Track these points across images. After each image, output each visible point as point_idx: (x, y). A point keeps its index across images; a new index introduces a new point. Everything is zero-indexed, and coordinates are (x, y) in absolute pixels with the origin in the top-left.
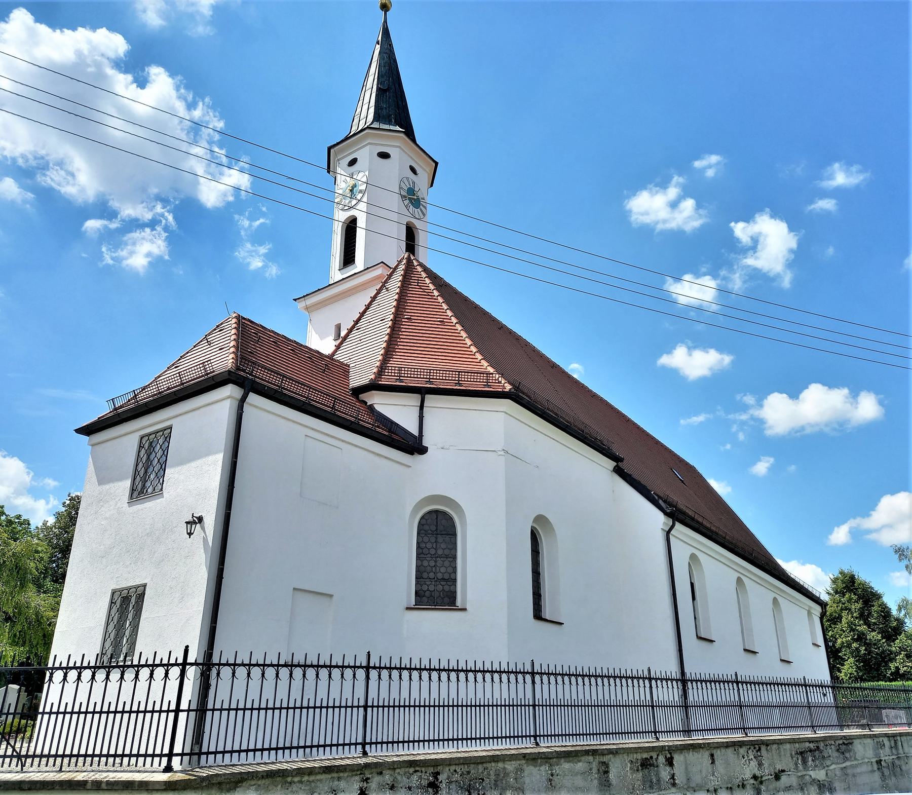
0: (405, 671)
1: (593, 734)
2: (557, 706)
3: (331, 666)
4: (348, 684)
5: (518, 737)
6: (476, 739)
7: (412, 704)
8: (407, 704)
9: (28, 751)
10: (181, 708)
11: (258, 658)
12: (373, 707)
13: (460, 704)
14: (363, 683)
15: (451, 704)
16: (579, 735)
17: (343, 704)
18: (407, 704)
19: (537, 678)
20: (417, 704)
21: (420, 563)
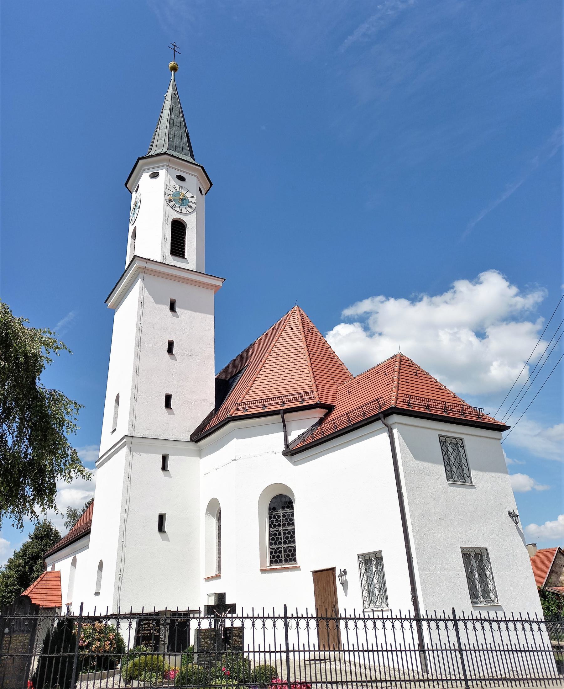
19: (461, 625)
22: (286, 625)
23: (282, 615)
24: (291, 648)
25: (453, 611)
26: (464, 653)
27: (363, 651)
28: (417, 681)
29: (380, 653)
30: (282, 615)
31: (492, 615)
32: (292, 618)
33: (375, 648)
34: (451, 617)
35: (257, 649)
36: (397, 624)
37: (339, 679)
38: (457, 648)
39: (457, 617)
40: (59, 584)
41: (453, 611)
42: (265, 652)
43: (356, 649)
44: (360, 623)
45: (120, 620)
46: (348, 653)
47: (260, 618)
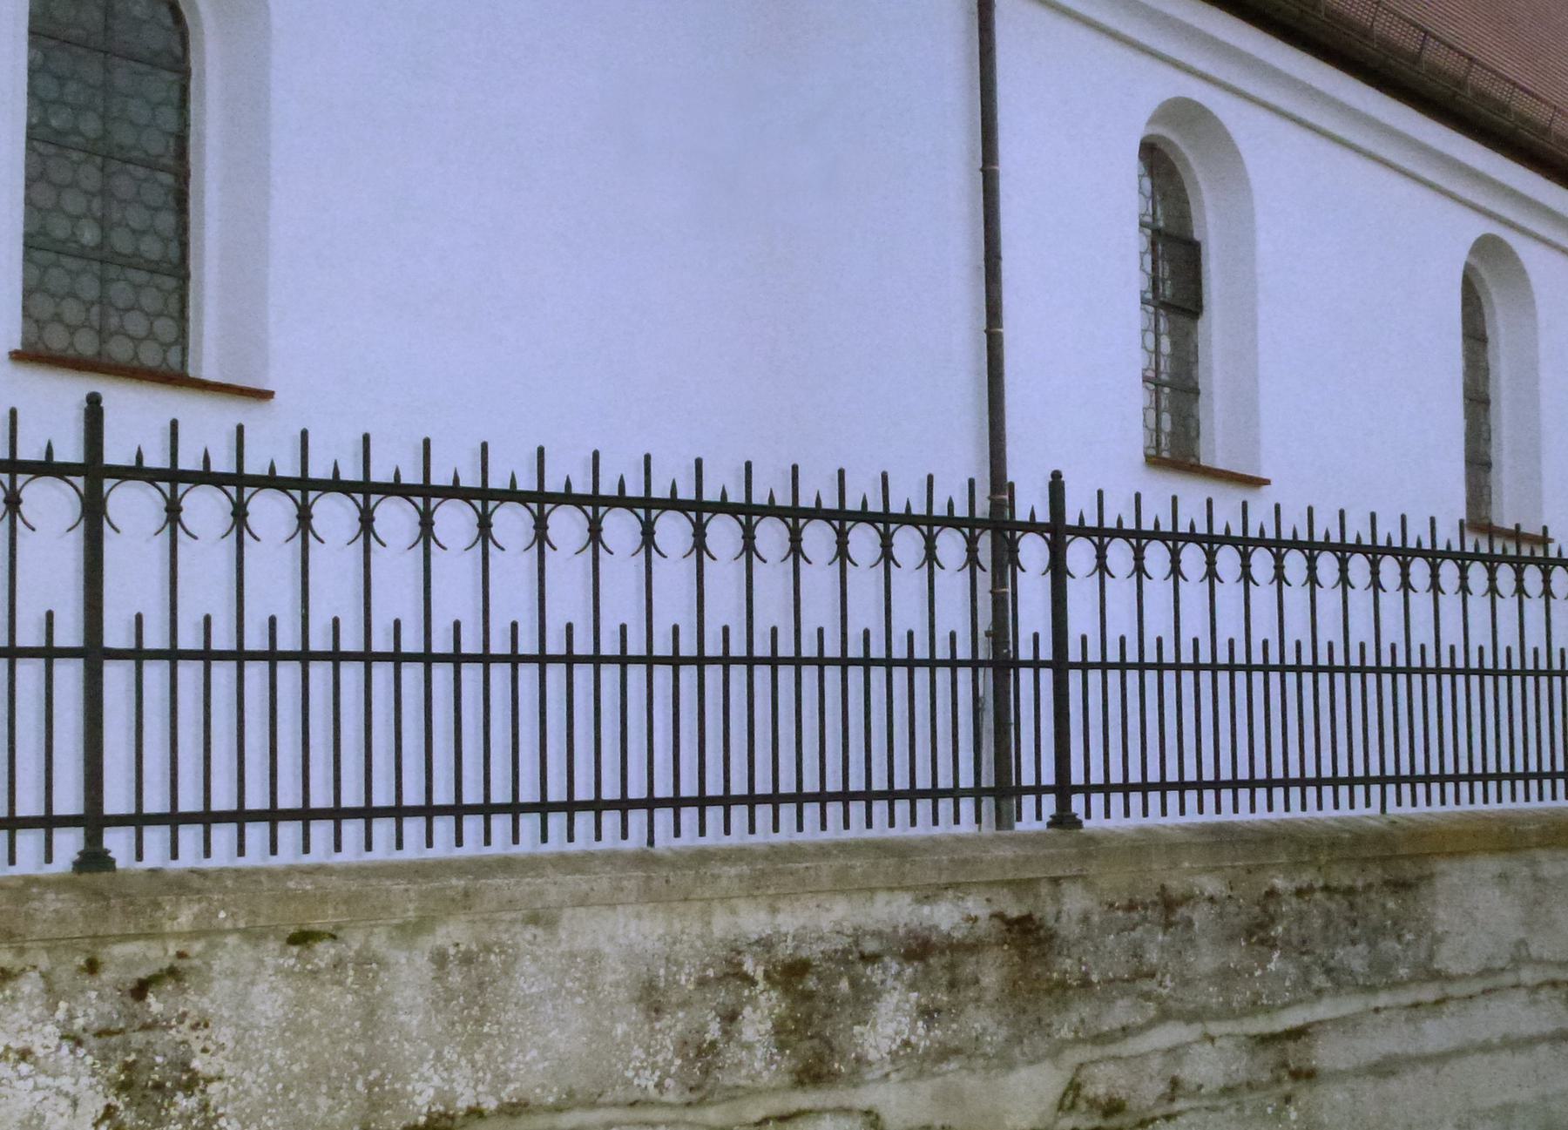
0: (1192, 546)
1: (1457, 778)
2: (1347, 670)
3: (174, 475)
4: (910, 581)
5: (1235, 784)
6: (1526, 776)
7: (809, 650)
8: (1307, 660)
9: (1107, 802)
10: (79, 663)
11: (568, 470)
12: (1085, 666)
13: (713, 648)
14: (72, 549)
15: (1386, 662)
16: (1442, 779)
17: (499, 646)
18: (832, 650)
19: (1079, 554)
20: (636, 647)
21: (49, 88)
22: (93, 513)
23: (70, 450)
24: (116, 635)
25: (1056, 487)
26: (1075, 677)
27: (1424, 671)
28: (1421, 779)
29: (878, 674)
30: (70, 450)
31: (1226, 518)
32: (136, 472)
33: (1205, 658)
34: (1043, 516)
35: (189, 639)
36: (1295, 562)
37: (901, 783)
38: (1046, 653)
39: (1071, 519)
40: (45, 307)
41: (1056, 487)
42: (597, 660)
43: (921, 652)
44: (1192, 557)
45: (80, 481)
46: (767, 669)
47: (219, 480)
